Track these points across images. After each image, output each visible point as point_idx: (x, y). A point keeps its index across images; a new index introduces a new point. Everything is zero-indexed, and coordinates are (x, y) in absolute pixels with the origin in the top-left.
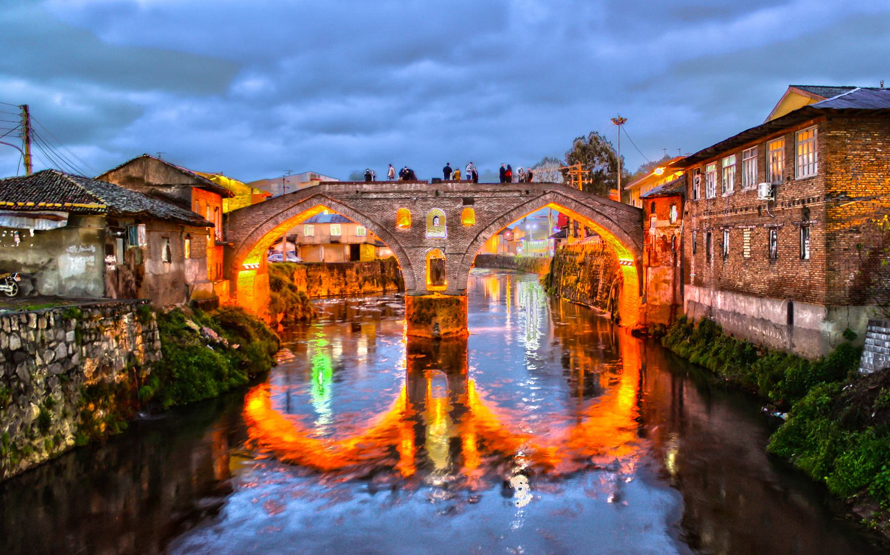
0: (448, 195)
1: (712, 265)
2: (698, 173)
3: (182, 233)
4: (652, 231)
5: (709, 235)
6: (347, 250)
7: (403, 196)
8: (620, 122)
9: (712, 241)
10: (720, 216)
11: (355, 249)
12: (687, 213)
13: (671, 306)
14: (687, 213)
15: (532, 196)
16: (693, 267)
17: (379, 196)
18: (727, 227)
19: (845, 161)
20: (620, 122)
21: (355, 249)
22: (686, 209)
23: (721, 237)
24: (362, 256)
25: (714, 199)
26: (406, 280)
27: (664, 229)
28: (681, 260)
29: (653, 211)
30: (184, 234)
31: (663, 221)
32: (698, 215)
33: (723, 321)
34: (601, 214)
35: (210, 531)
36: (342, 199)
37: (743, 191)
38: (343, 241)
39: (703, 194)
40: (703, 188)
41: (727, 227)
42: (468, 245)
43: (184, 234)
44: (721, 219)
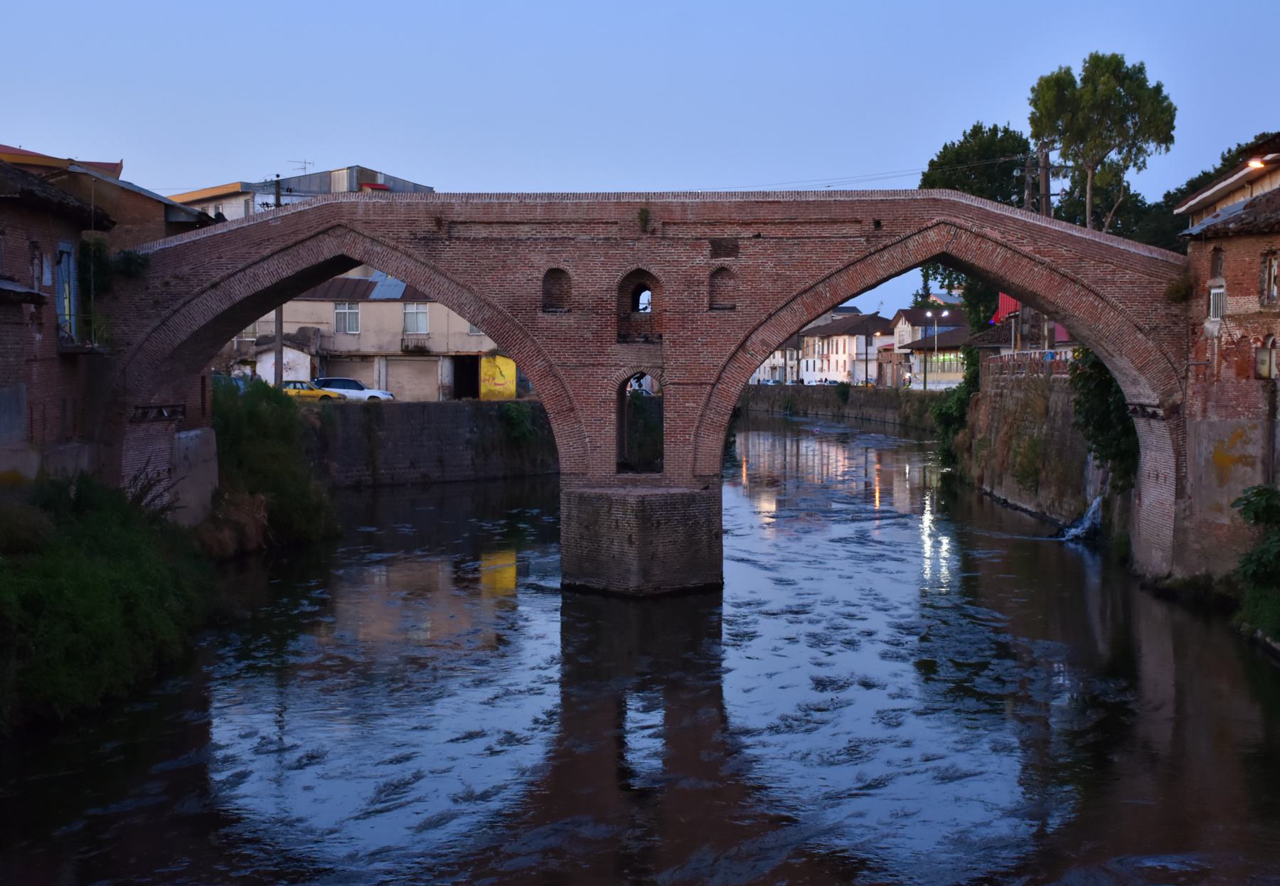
0: (671, 231)
4: (1212, 325)
6: (444, 372)
7: (557, 234)
15: (891, 235)
17: (496, 232)
19: (1080, 413)
21: (466, 368)
26: (562, 450)
27: (1239, 319)
29: (1215, 273)
31: (1242, 300)
34: (1074, 281)
35: (731, 657)
36: (398, 239)
38: (437, 346)
42: (722, 362)
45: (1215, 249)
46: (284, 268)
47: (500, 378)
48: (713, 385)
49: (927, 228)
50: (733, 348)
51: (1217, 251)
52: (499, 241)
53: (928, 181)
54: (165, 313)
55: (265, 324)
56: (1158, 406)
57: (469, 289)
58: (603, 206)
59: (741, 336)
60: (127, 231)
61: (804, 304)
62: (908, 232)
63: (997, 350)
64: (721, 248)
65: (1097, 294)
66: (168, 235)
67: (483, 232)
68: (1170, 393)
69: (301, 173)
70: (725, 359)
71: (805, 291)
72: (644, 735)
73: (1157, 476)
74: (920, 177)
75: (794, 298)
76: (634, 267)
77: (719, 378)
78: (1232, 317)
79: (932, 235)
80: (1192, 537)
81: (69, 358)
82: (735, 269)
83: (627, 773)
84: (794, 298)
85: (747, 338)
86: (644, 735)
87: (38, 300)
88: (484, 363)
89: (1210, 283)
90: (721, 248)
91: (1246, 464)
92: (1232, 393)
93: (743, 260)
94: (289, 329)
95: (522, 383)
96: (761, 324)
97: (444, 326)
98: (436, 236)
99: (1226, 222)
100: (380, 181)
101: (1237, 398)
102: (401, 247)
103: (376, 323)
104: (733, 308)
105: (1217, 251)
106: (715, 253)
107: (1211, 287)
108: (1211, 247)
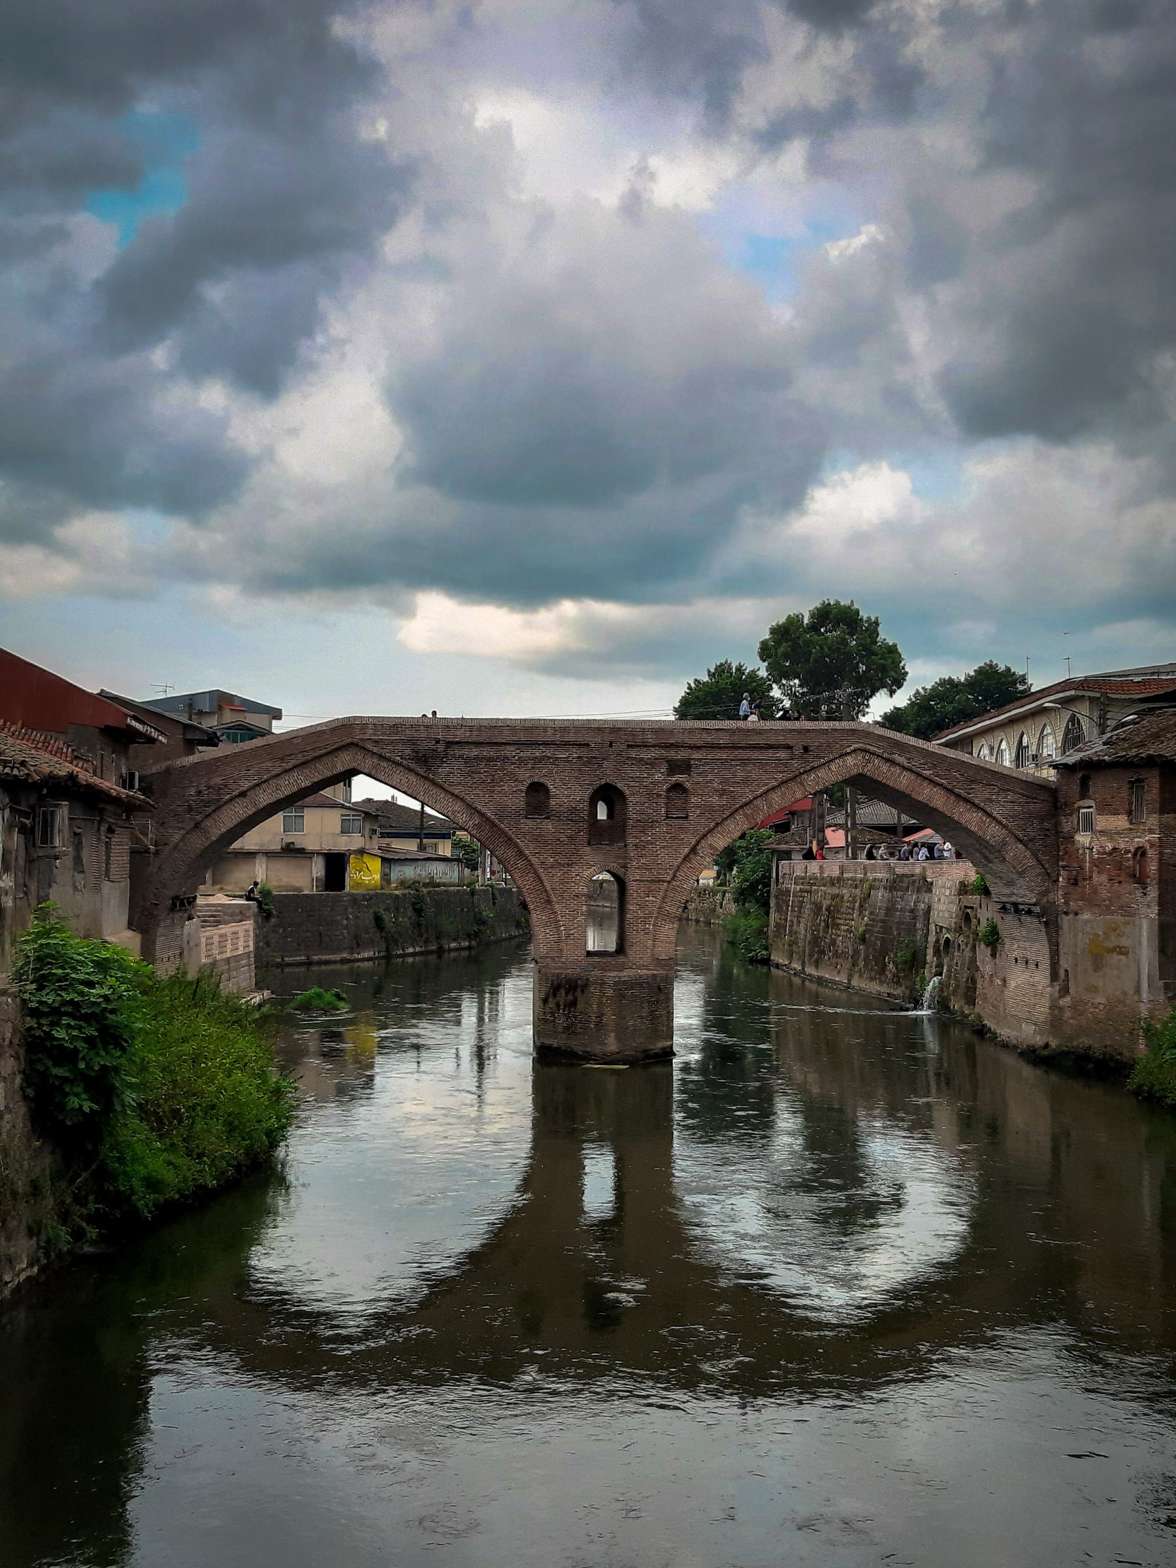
3: (100, 822)
6: (318, 868)
21: (336, 864)
29: (1084, 795)
30: (104, 828)
31: (1112, 818)
45: (1083, 776)
48: (669, 882)
49: (847, 754)
50: (687, 850)
52: (490, 760)
53: (686, 708)
54: (199, 818)
56: (1035, 905)
58: (545, 729)
59: (693, 842)
61: (745, 815)
62: (831, 757)
64: (675, 767)
65: (985, 812)
67: (475, 752)
68: (1045, 893)
69: (161, 696)
70: (680, 860)
71: (746, 804)
72: (599, 1182)
73: (1027, 962)
75: (736, 810)
76: (603, 782)
77: (674, 876)
79: (850, 760)
80: (1068, 1014)
82: (688, 785)
84: (736, 810)
85: (698, 843)
86: (599, 1182)
89: (1081, 803)
91: (1121, 953)
92: (1104, 894)
93: (696, 778)
96: (710, 831)
101: (1110, 899)
102: (405, 762)
107: (1080, 808)
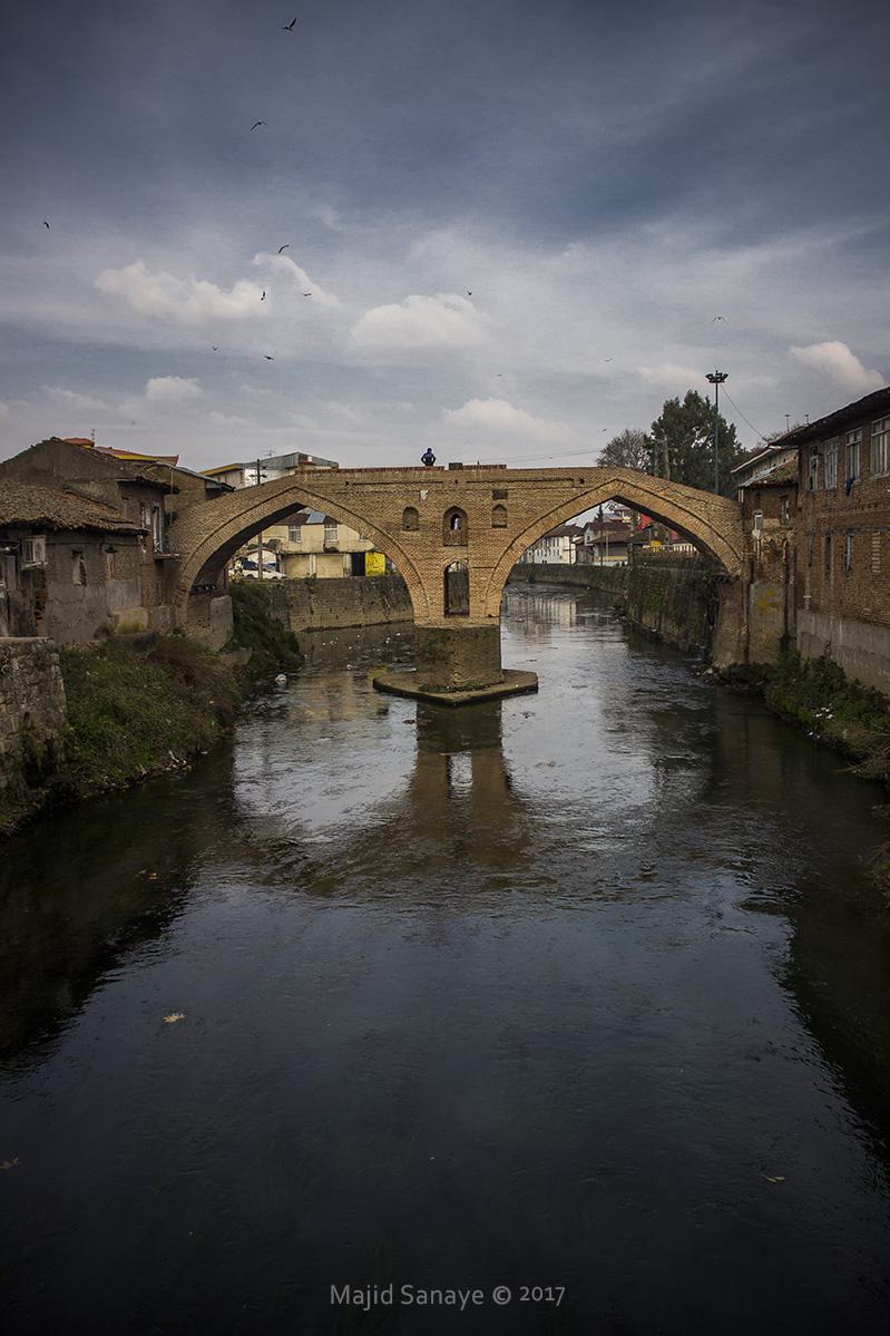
1: (832, 583)
2: (815, 453)
5: (829, 540)
8: (717, 379)
9: (832, 549)
10: (842, 514)
11: (358, 559)
12: (800, 510)
13: (781, 640)
14: (800, 510)
16: (808, 585)
18: (851, 530)
20: (717, 379)
21: (358, 559)
22: (800, 504)
23: (843, 544)
24: (367, 570)
25: (834, 490)
27: (771, 531)
28: (795, 575)
29: (758, 507)
30: (105, 547)
31: (771, 521)
32: (815, 511)
33: (843, 661)
37: (872, 479)
39: (822, 482)
40: (822, 474)
41: (851, 530)
43: (105, 547)
44: (843, 519)
46: (267, 510)
47: (376, 564)
51: (758, 495)
55: (254, 541)
57: (364, 519)
60: (187, 494)
63: (641, 545)
64: (498, 495)
66: (207, 500)
74: (658, 414)
78: (766, 530)
81: (159, 562)
83: (450, 792)
87: (145, 533)
88: (367, 554)
90: (498, 495)
94: (265, 541)
95: (388, 566)
97: (347, 537)
98: (349, 489)
99: (762, 480)
100: (310, 460)
103: (312, 536)
104: (505, 526)
105: (758, 495)
106: (495, 497)
108: (755, 493)
